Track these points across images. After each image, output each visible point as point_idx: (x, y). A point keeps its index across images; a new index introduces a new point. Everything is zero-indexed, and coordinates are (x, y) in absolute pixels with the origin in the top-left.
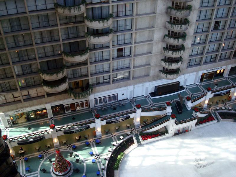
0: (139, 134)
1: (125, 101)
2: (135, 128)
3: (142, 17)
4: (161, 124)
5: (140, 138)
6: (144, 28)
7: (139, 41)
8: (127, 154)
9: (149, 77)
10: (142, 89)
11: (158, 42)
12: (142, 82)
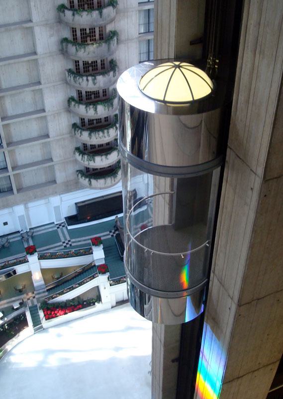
0: (39, 305)
1: (9, 237)
2: (35, 292)
3: (15, 63)
4: (80, 284)
5: (41, 314)
6: (18, 86)
7: (14, 114)
8: (9, 350)
9: (54, 185)
10: (49, 210)
11: (59, 114)
12: (44, 196)
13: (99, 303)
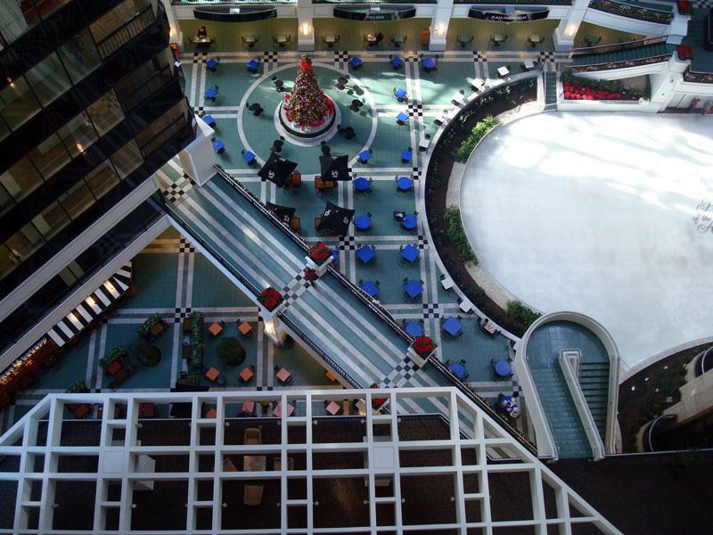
0: (559, 74)
5: (559, 90)
13: (646, 99)
